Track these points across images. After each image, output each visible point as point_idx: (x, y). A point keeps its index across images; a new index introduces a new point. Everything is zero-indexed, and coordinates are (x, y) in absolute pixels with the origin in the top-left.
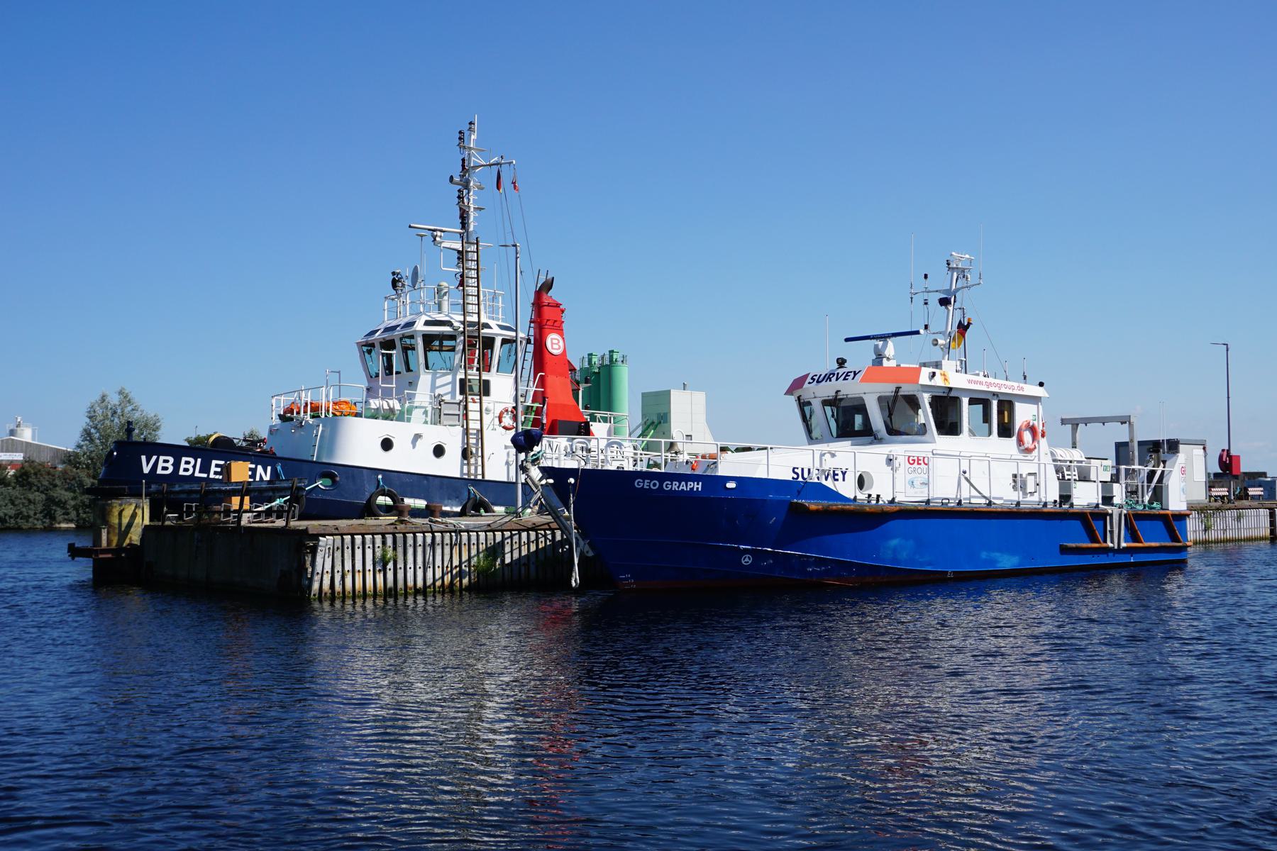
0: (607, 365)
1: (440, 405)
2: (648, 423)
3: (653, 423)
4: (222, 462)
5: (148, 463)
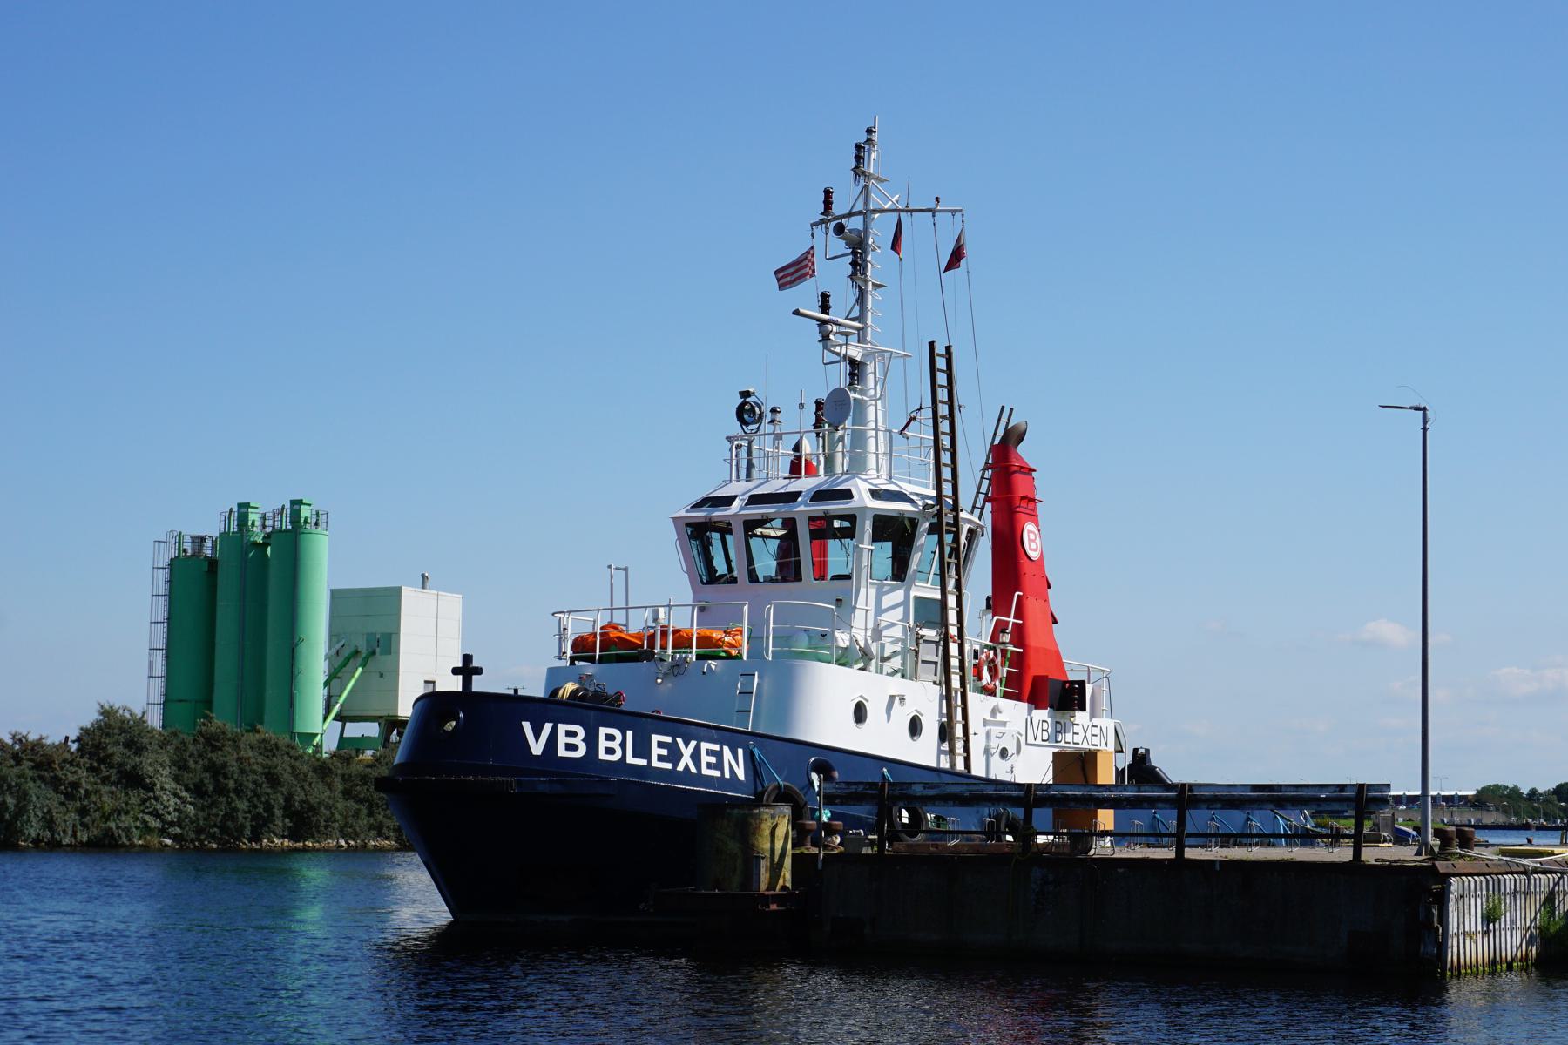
0: (287, 531)
1: (917, 644)
2: (347, 652)
3: (356, 653)
4: (668, 739)
5: (537, 737)
